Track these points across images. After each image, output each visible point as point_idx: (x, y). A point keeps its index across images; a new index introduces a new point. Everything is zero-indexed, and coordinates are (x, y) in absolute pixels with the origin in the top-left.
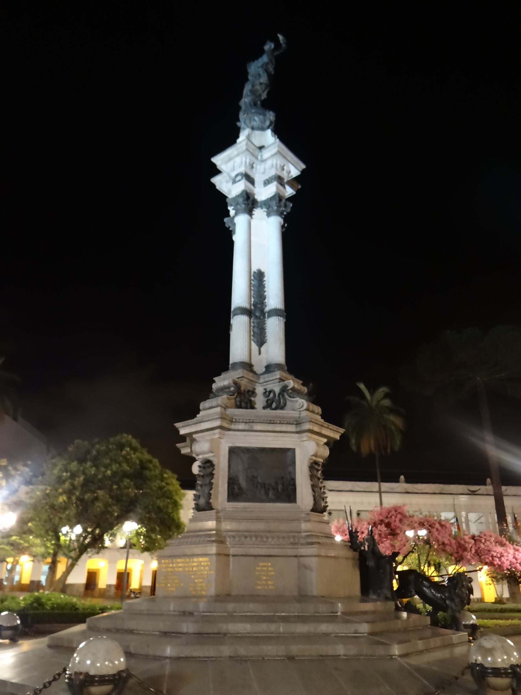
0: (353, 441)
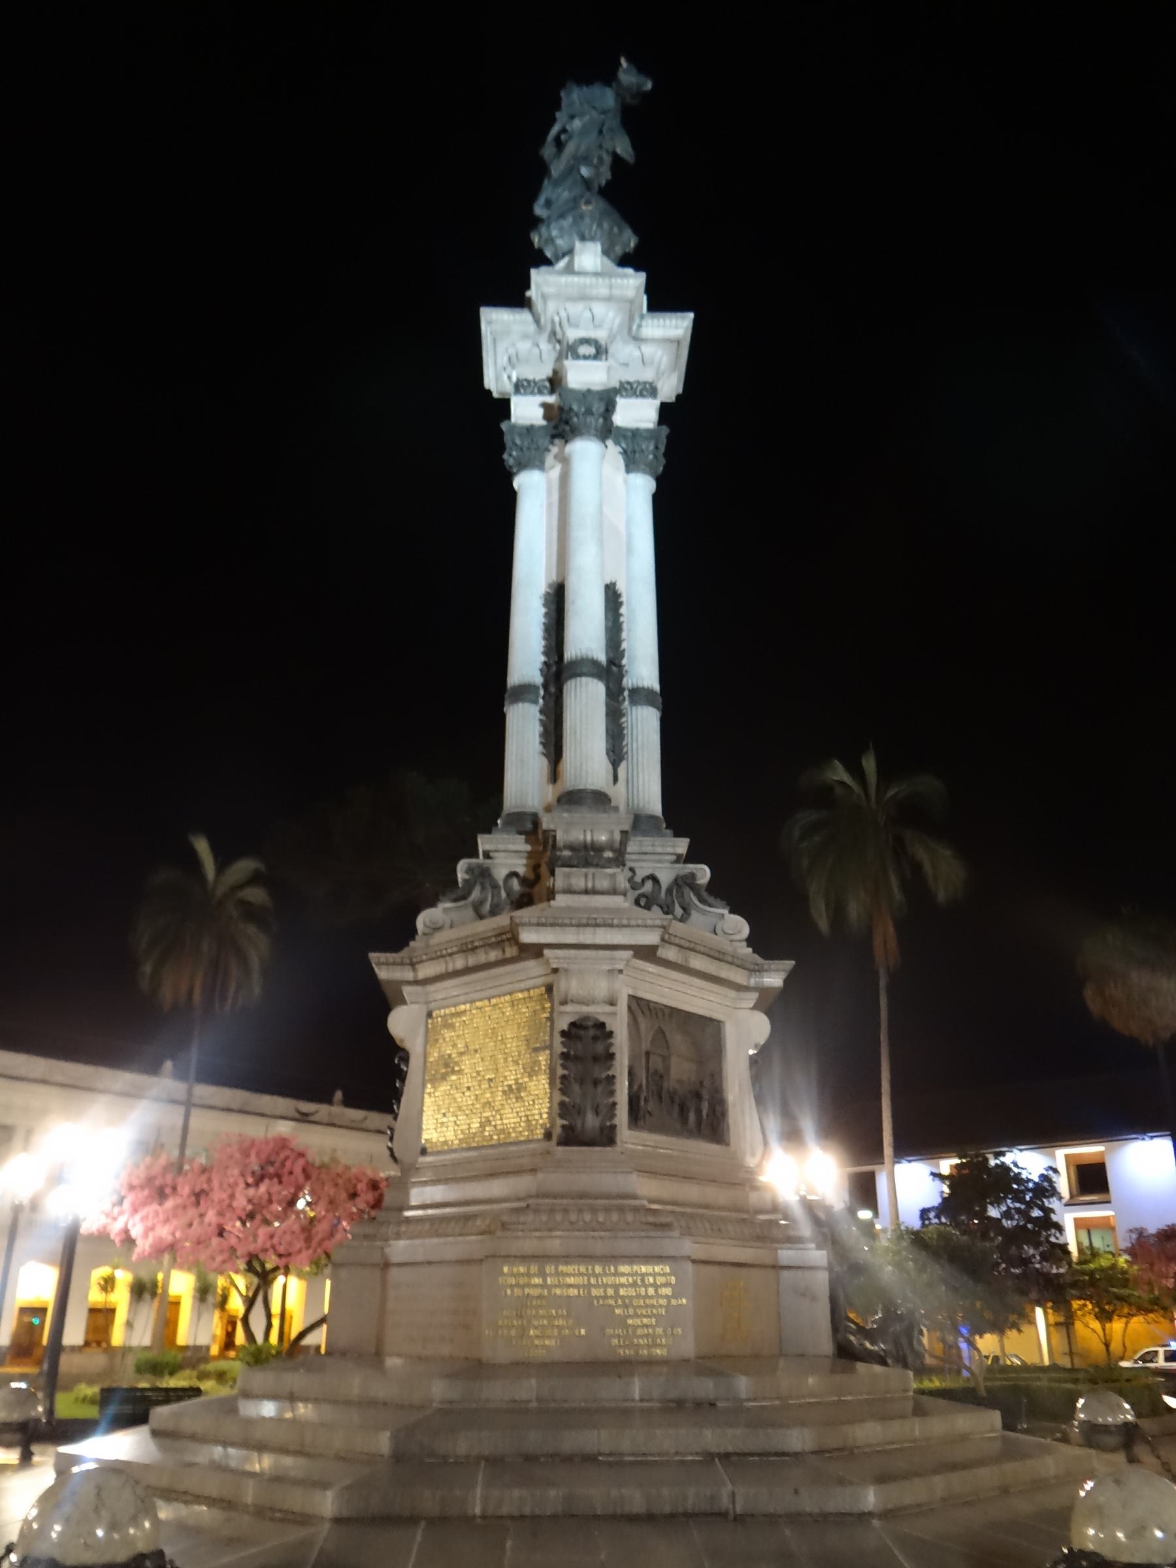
0: (148, 968)
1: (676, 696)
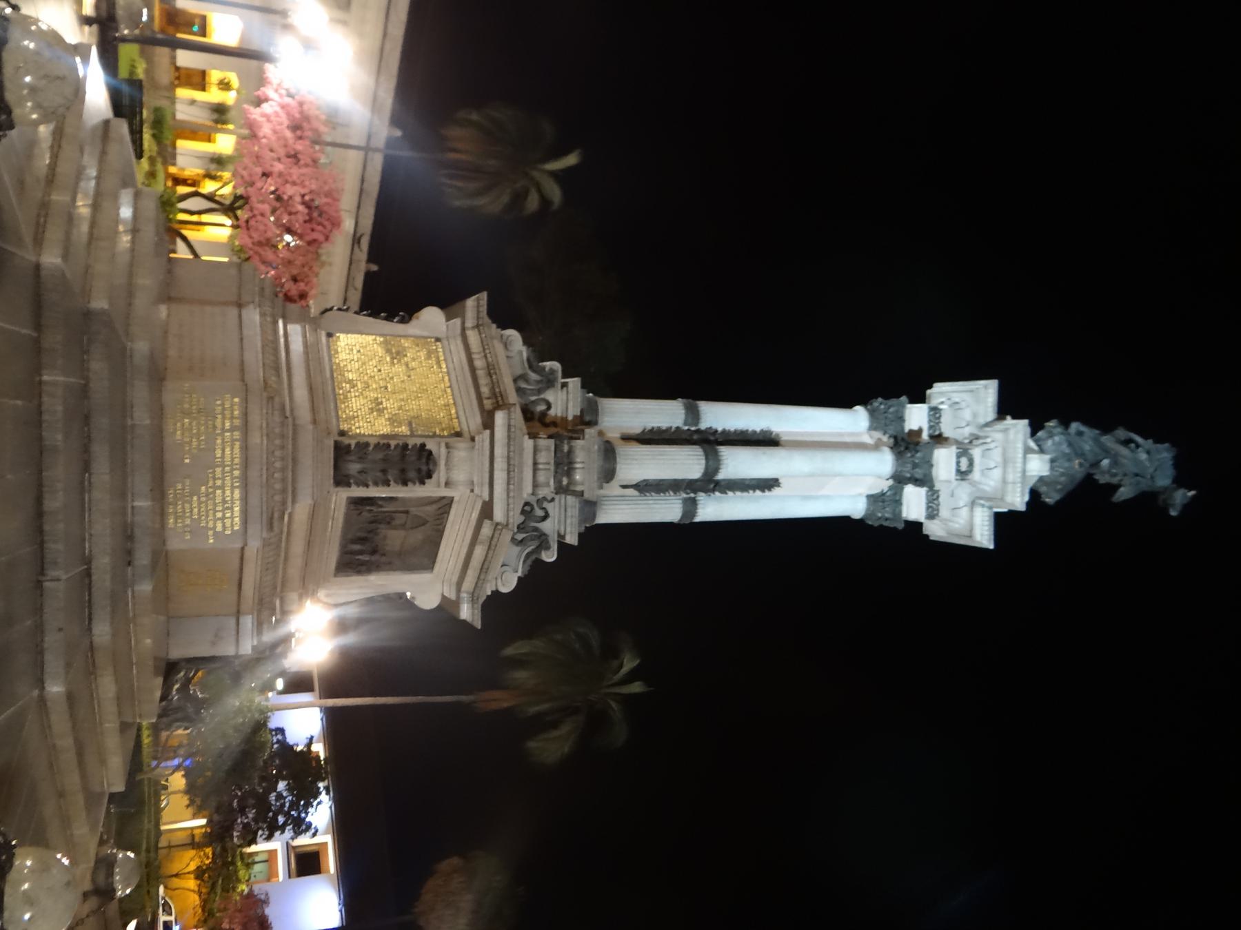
1: (691, 536)
